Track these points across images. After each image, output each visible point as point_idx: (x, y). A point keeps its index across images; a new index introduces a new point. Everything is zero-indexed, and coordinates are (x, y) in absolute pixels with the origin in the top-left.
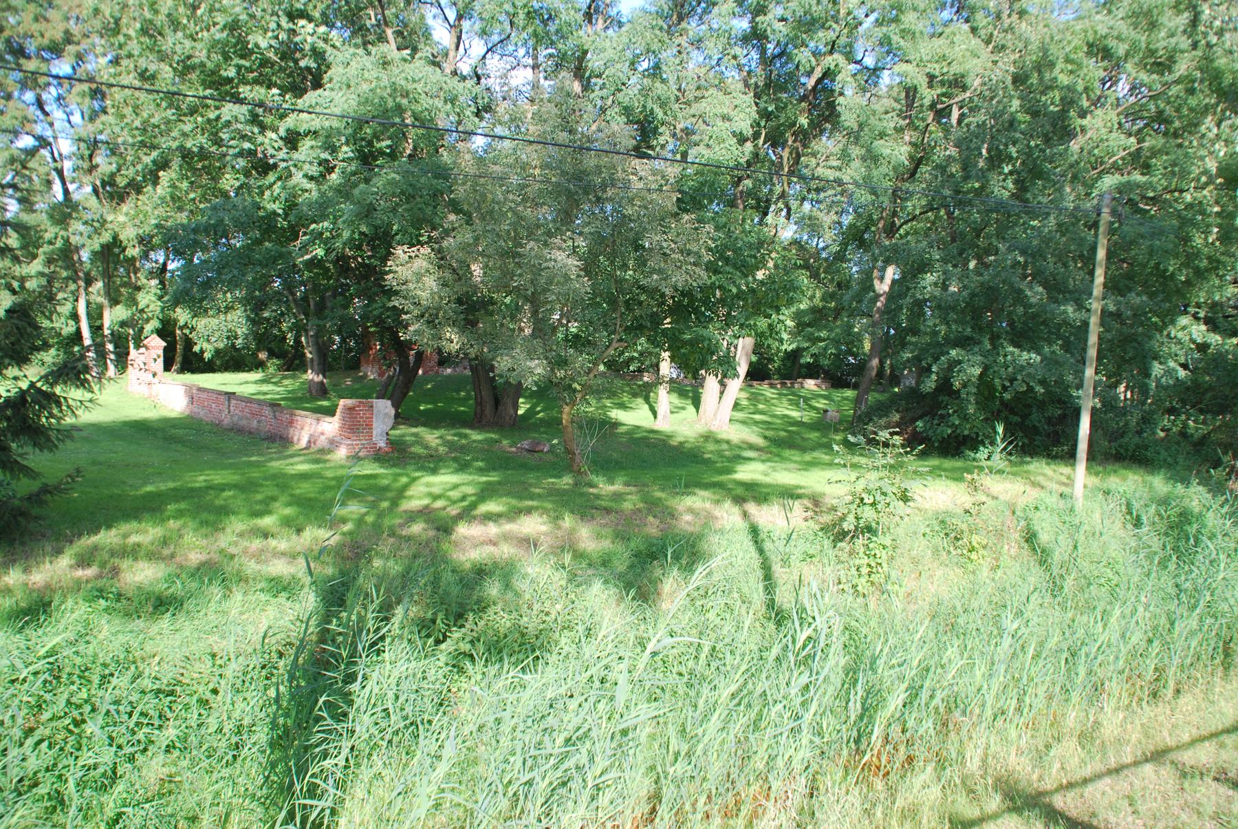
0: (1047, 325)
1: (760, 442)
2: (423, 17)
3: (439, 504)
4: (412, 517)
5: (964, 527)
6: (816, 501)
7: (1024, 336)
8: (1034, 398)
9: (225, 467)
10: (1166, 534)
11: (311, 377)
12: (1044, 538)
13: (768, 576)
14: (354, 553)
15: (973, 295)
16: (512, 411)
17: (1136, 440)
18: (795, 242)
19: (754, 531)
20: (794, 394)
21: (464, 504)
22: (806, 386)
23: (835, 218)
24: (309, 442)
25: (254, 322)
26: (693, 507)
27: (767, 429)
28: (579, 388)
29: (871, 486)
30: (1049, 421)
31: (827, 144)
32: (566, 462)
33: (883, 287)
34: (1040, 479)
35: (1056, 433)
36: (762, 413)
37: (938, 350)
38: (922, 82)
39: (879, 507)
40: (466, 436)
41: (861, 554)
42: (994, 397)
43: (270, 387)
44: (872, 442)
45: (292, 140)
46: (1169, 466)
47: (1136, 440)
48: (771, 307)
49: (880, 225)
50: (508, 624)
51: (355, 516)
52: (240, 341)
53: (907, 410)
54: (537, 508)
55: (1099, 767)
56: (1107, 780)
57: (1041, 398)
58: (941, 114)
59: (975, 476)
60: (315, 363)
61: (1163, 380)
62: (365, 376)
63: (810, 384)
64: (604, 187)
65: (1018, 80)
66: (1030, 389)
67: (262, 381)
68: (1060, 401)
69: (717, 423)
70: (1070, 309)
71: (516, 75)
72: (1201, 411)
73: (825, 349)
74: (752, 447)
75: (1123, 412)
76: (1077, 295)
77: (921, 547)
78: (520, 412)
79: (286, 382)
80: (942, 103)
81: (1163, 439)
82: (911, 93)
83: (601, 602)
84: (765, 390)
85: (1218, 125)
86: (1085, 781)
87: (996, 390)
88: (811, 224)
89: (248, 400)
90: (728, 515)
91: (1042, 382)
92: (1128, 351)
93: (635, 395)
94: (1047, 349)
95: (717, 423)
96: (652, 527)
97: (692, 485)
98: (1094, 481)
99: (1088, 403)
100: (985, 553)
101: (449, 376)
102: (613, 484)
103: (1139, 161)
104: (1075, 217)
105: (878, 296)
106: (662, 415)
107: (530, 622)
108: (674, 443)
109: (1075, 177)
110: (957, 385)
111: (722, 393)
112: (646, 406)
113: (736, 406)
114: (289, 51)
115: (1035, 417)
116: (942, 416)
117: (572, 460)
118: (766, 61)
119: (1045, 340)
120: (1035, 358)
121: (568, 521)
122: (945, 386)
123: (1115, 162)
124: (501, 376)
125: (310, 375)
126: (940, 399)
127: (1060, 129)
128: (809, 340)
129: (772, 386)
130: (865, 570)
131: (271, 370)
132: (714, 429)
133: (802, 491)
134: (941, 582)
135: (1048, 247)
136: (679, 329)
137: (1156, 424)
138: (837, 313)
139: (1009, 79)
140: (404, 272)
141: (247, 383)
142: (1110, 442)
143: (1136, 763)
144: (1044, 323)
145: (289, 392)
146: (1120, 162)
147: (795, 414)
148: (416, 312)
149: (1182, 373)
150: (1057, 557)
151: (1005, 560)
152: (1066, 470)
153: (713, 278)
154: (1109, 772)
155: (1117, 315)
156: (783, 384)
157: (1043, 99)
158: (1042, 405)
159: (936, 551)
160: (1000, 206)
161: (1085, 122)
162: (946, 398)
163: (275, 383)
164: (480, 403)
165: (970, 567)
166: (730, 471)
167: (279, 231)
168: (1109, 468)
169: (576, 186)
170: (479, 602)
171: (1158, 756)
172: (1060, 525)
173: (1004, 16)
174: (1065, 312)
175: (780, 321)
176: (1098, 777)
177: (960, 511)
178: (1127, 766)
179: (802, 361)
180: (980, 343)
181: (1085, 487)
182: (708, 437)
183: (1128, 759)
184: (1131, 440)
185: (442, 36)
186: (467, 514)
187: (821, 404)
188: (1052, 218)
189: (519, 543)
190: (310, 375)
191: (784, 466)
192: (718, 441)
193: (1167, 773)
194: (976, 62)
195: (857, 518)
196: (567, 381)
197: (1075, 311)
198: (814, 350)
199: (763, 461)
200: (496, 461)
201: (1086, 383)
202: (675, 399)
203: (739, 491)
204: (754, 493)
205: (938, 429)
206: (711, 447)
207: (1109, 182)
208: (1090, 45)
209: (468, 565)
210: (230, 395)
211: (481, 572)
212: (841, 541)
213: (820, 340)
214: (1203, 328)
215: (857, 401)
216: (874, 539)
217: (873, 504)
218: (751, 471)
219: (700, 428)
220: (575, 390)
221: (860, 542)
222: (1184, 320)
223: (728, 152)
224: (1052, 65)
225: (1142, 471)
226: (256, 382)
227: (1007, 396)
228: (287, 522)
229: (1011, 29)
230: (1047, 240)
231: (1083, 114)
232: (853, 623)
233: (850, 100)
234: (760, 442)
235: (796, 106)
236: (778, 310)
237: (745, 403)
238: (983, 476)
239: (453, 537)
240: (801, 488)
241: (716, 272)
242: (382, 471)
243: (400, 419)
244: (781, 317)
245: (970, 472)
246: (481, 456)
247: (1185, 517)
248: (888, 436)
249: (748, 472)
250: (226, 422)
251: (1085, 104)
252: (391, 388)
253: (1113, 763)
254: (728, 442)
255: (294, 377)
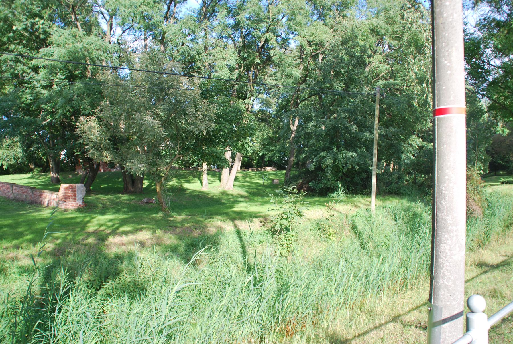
0: (359, 141)
1: (246, 194)
2: (96, 18)
3: (102, 228)
4: (89, 234)
5: (327, 225)
6: (265, 218)
7: (351, 146)
8: (356, 171)
9: (9, 217)
10: (408, 223)
11: (52, 175)
12: (360, 228)
13: (244, 252)
14: (59, 253)
15: (329, 130)
16: (139, 185)
17: (396, 185)
18: (260, 111)
19: (238, 232)
20: (261, 173)
21: (113, 228)
22: (267, 170)
23: (276, 100)
24: (48, 203)
25: (25, 151)
26: (215, 223)
27: (249, 189)
28: (163, 175)
29: (286, 211)
30: (362, 180)
31: (270, 70)
32: (159, 207)
33: (294, 128)
34: (359, 204)
35: (365, 184)
36: (248, 182)
37: (316, 153)
38: (305, 44)
39: (289, 219)
40: (119, 198)
41: (283, 240)
42: (340, 171)
43: (35, 180)
44: (286, 192)
45: (36, 69)
46: (409, 195)
47: (396, 185)
48: (243, 138)
49: (292, 103)
50: (129, 280)
51: (63, 236)
52: (20, 160)
53: (305, 178)
54: (145, 228)
55: (371, 326)
56: (375, 331)
57: (358, 171)
58: (315, 57)
59: (330, 204)
60: (54, 169)
61: (406, 161)
62: (78, 174)
63: (269, 169)
64: (169, 88)
65: (343, 43)
66: (353, 167)
67: (31, 178)
68: (366, 172)
69: (228, 187)
70: (367, 134)
71: (137, 43)
72: (420, 173)
73: (274, 154)
74: (242, 196)
75: (391, 174)
76: (370, 128)
77: (309, 235)
78: (144, 186)
79: (42, 178)
80: (314, 52)
81: (406, 185)
82: (301, 49)
83: (175, 268)
84: (250, 173)
85: (414, 59)
86: (366, 333)
87: (340, 168)
88: (267, 103)
89: (20, 186)
90: (228, 227)
91: (358, 164)
92: (390, 150)
93: (194, 177)
94: (359, 151)
95: (228, 187)
96: (196, 233)
97: (211, 215)
98: (380, 203)
99: (375, 171)
100: (336, 235)
101: (114, 172)
102: (180, 215)
103: (393, 74)
104: (368, 97)
105: (292, 131)
106: (205, 185)
107: (139, 279)
108: (209, 196)
109: (367, 83)
110: (324, 166)
111: (229, 174)
112: (199, 181)
113: (236, 179)
114: (32, 31)
115: (356, 178)
116: (319, 180)
117: (162, 206)
118: (244, 37)
119: (358, 147)
120: (355, 154)
121: (159, 232)
122: (319, 168)
123: (383, 75)
124: (127, 171)
125: (52, 174)
126: (318, 173)
127: (361, 63)
128: (268, 150)
129: (253, 170)
130: (285, 246)
131: (36, 173)
132: (226, 190)
133: (259, 214)
134: (317, 249)
135: (358, 110)
136: (203, 148)
137: (403, 179)
138: (279, 139)
139: (340, 43)
140: (85, 128)
141: (24, 178)
142: (386, 187)
143: (386, 323)
144: (358, 140)
145: (43, 182)
146: (385, 75)
147: (261, 182)
148: (91, 145)
149: (413, 158)
150: (365, 236)
151: (344, 238)
152: (369, 199)
153: (218, 126)
154: (376, 328)
155: (386, 136)
156: (257, 170)
157: (353, 50)
158: (359, 173)
159: (315, 236)
160: (338, 94)
161: (371, 60)
162: (321, 172)
163: (37, 178)
164: (126, 184)
165: (330, 242)
166: (232, 207)
167: (32, 110)
168: (386, 197)
169: (159, 89)
170: (116, 270)
171: (395, 319)
172: (366, 222)
173: (337, 18)
174: (365, 135)
175: (246, 143)
176: (371, 330)
177: (325, 219)
178: (383, 324)
179: (266, 160)
180: (332, 149)
181: (376, 205)
182: (224, 193)
183: (383, 322)
184: (394, 186)
185: (104, 26)
186: (114, 233)
187: (272, 177)
188: (358, 98)
189: (137, 244)
190: (52, 174)
191: (255, 204)
192: (228, 195)
193: (398, 325)
194: (326, 35)
195: (281, 225)
196: (158, 173)
197: (369, 135)
198: (270, 155)
199: (247, 202)
200: (131, 208)
201: (374, 164)
202: (210, 177)
203: (234, 215)
204: (241, 216)
205: (315, 185)
206: (225, 197)
207: (381, 83)
208: (370, 30)
209: (112, 255)
210: (13, 185)
211: (119, 258)
212: (275, 234)
213: (272, 150)
214: (421, 140)
215: (286, 175)
216: (288, 233)
217: (287, 218)
218: (241, 207)
219: (221, 190)
220: (161, 176)
221: (282, 234)
222: (413, 137)
223: (223, 74)
224: (356, 37)
225: (398, 198)
226: (28, 178)
227: (345, 171)
228: (30, 241)
229: (339, 23)
230: (357, 107)
231: (370, 56)
232: (281, 269)
233: (276, 52)
234: (246, 194)
235: (255, 55)
236: (245, 138)
237: (241, 178)
238: (333, 204)
239: (106, 243)
240: (261, 213)
241: (218, 124)
242: (81, 215)
243: (89, 192)
244: (247, 141)
245: (328, 202)
246: (125, 206)
247: (415, 215)
248: (292, 190)
249: (240, 207)
250: (11, 196)
251: (370, 52)
252: (86, 180)
253: (377, 324)
254: (232, 195)
255: (46, 175)
